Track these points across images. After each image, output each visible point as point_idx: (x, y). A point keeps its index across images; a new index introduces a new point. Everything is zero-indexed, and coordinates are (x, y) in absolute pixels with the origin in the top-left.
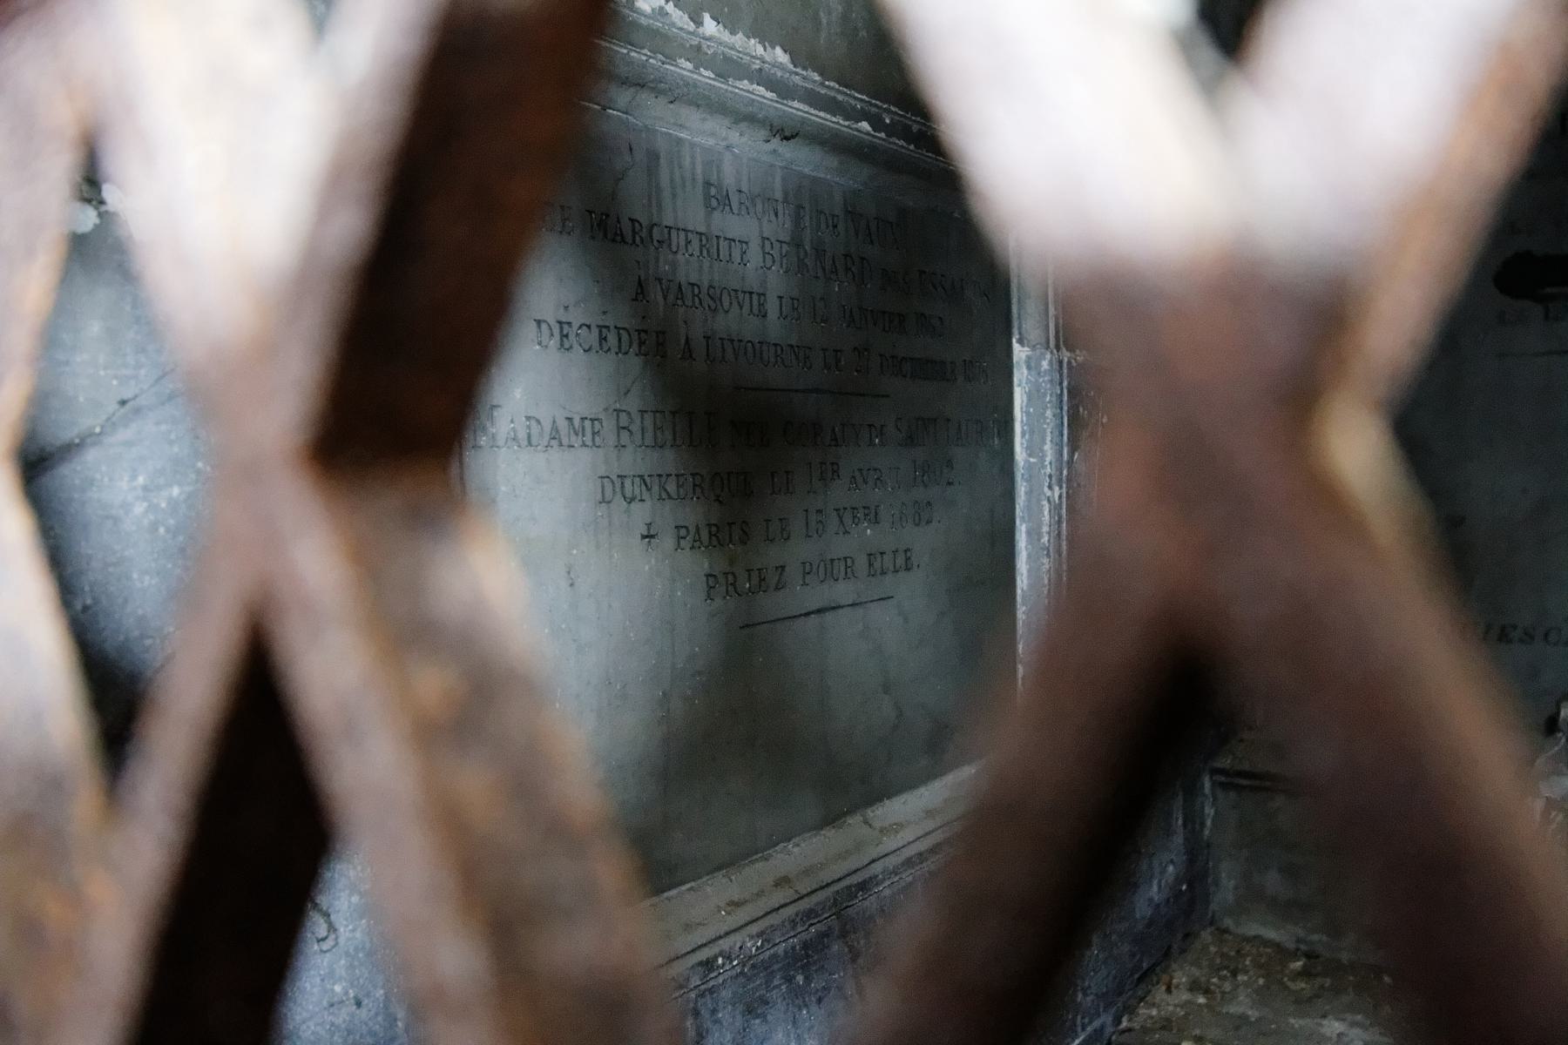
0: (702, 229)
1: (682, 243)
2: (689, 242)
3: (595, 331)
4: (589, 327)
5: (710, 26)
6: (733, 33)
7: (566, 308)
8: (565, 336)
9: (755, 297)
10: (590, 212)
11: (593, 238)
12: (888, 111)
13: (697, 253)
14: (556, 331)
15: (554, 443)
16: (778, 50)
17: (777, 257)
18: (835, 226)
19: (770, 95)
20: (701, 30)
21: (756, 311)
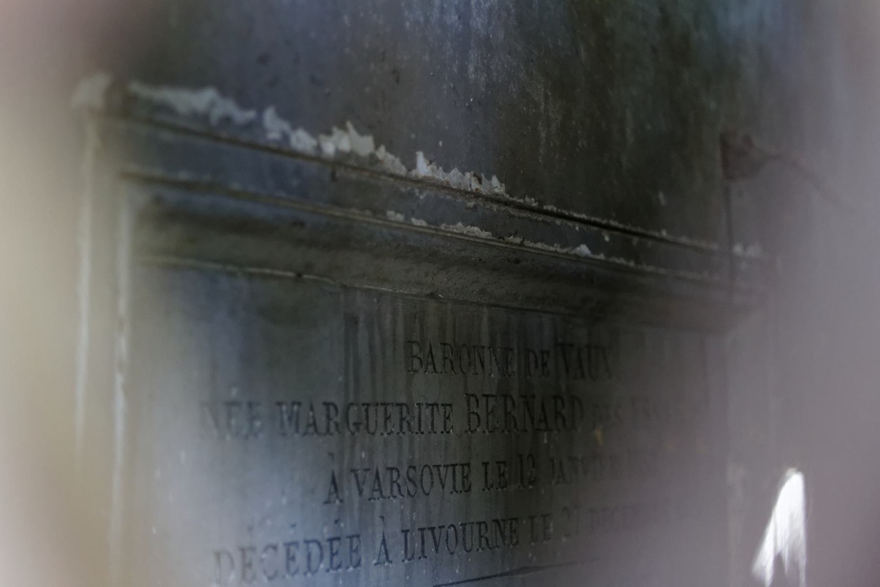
0: (403, 399)
1: (381, 421)
2: (387, 418)
3: (282, 551)
4: (275, 548)
5: (423, 168)
6: (447, 170)
7: (250, 529)
8: (247, 565)
9: (436, 531)
10: (280, 404)
11: (284, 434)
12: (607, 227)
13: (396, 429)
14: (238, 562)
15: (311, 429)
16: (495, 181)
17: (483, 416)
18: (544, 365)
19: (485, 234)
20: (413, 173)
21: (459, 487)
